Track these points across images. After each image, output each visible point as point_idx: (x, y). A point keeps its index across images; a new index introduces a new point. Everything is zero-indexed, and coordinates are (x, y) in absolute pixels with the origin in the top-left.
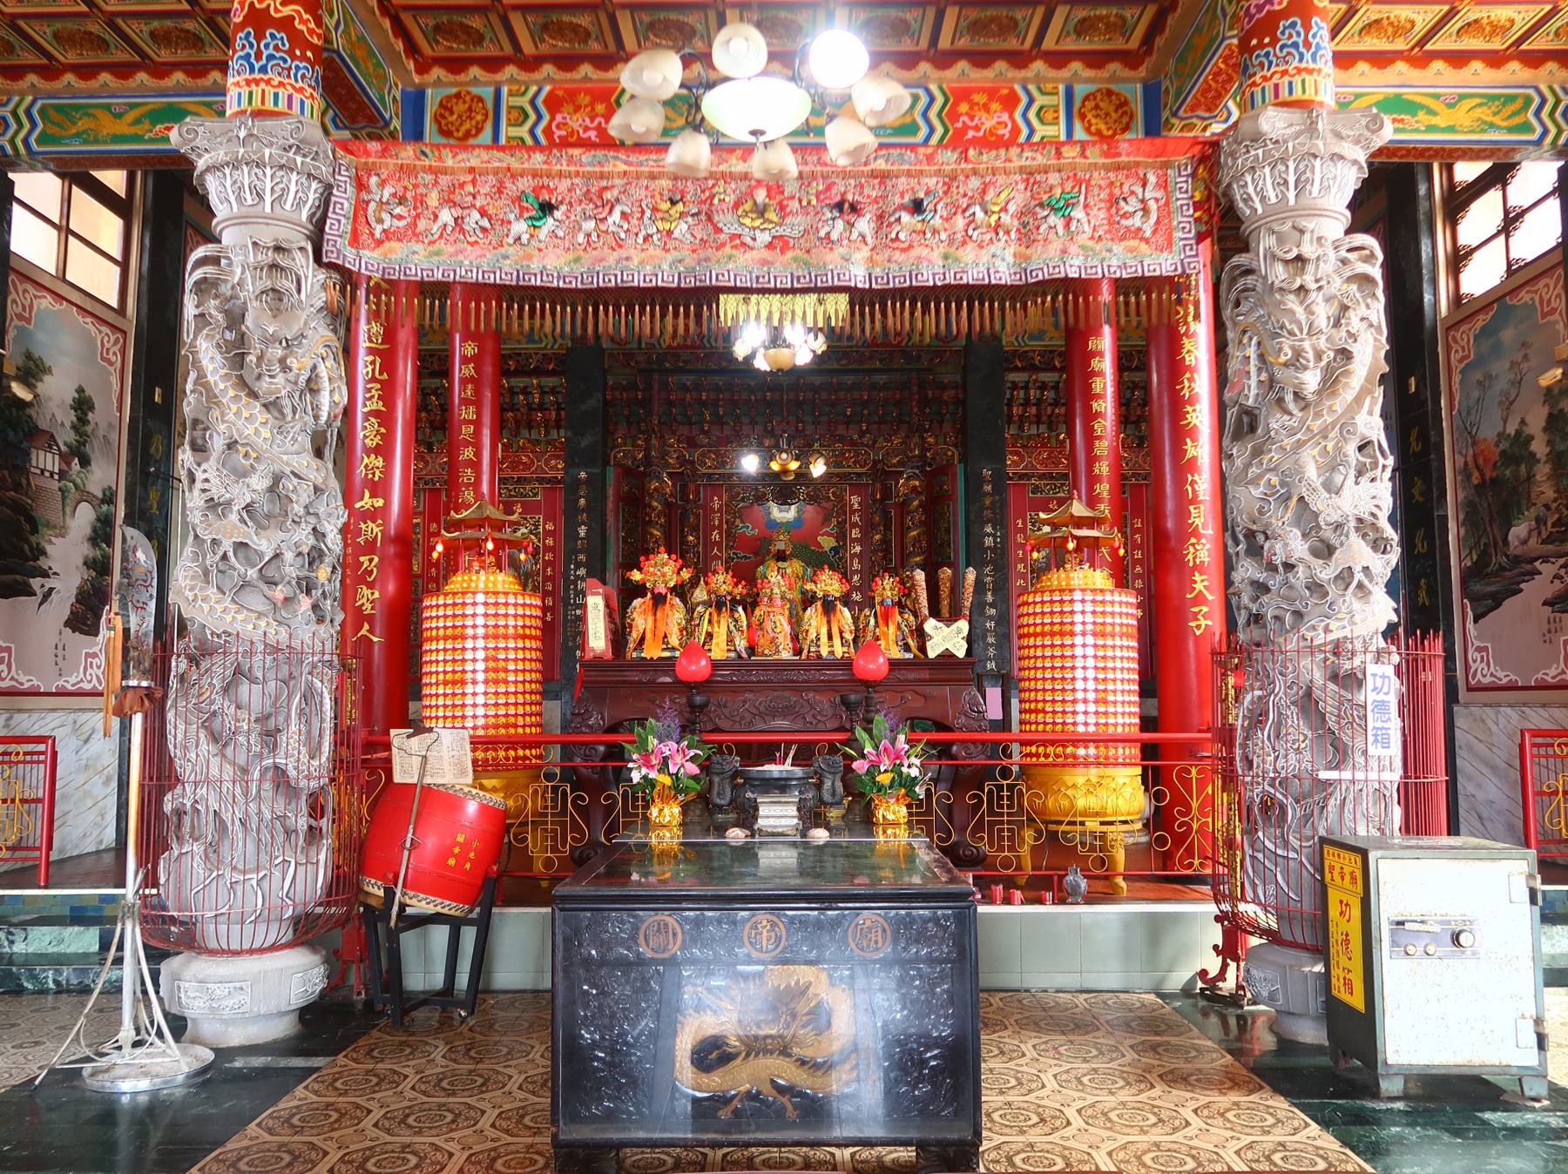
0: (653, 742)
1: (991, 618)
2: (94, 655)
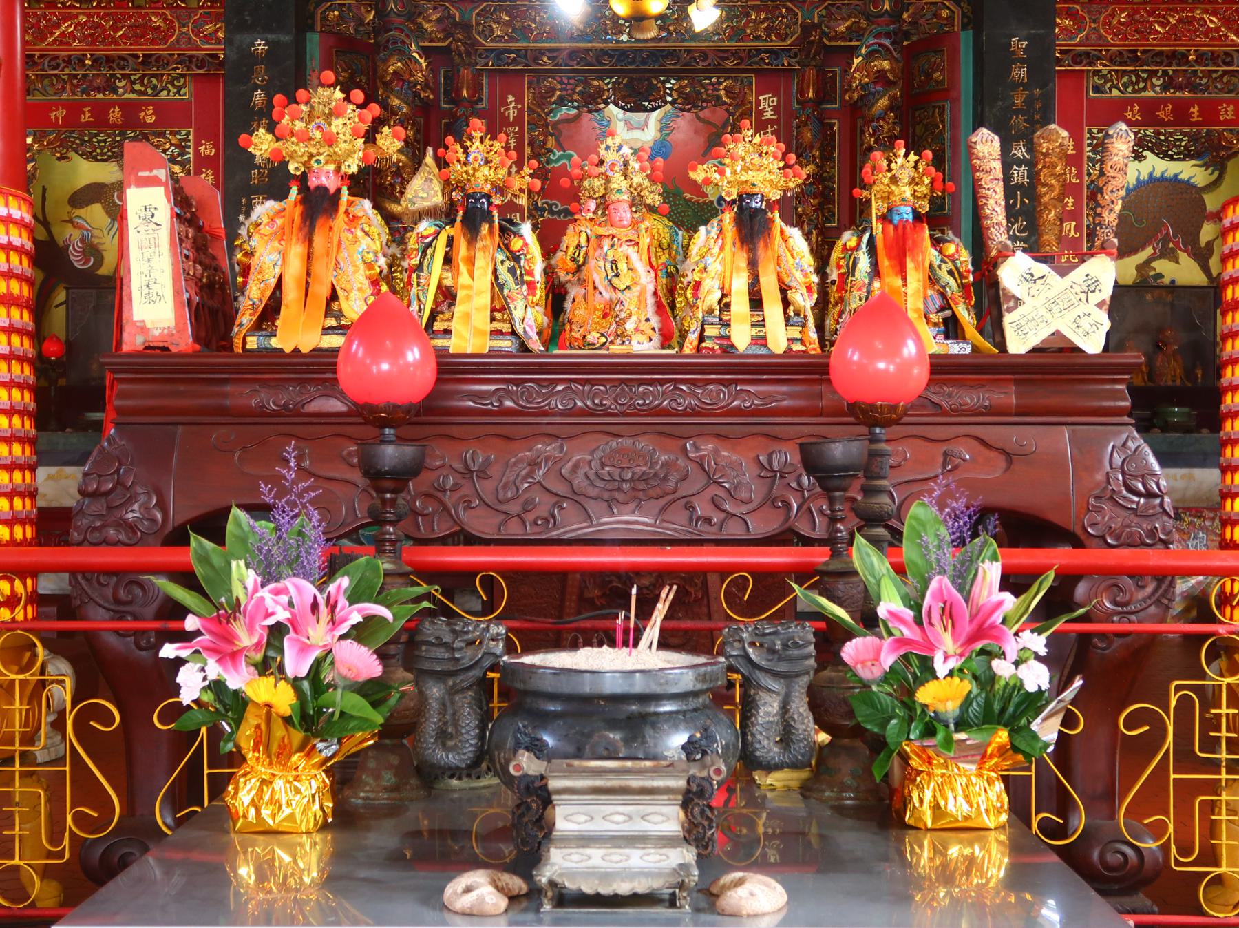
0: (243, 577)
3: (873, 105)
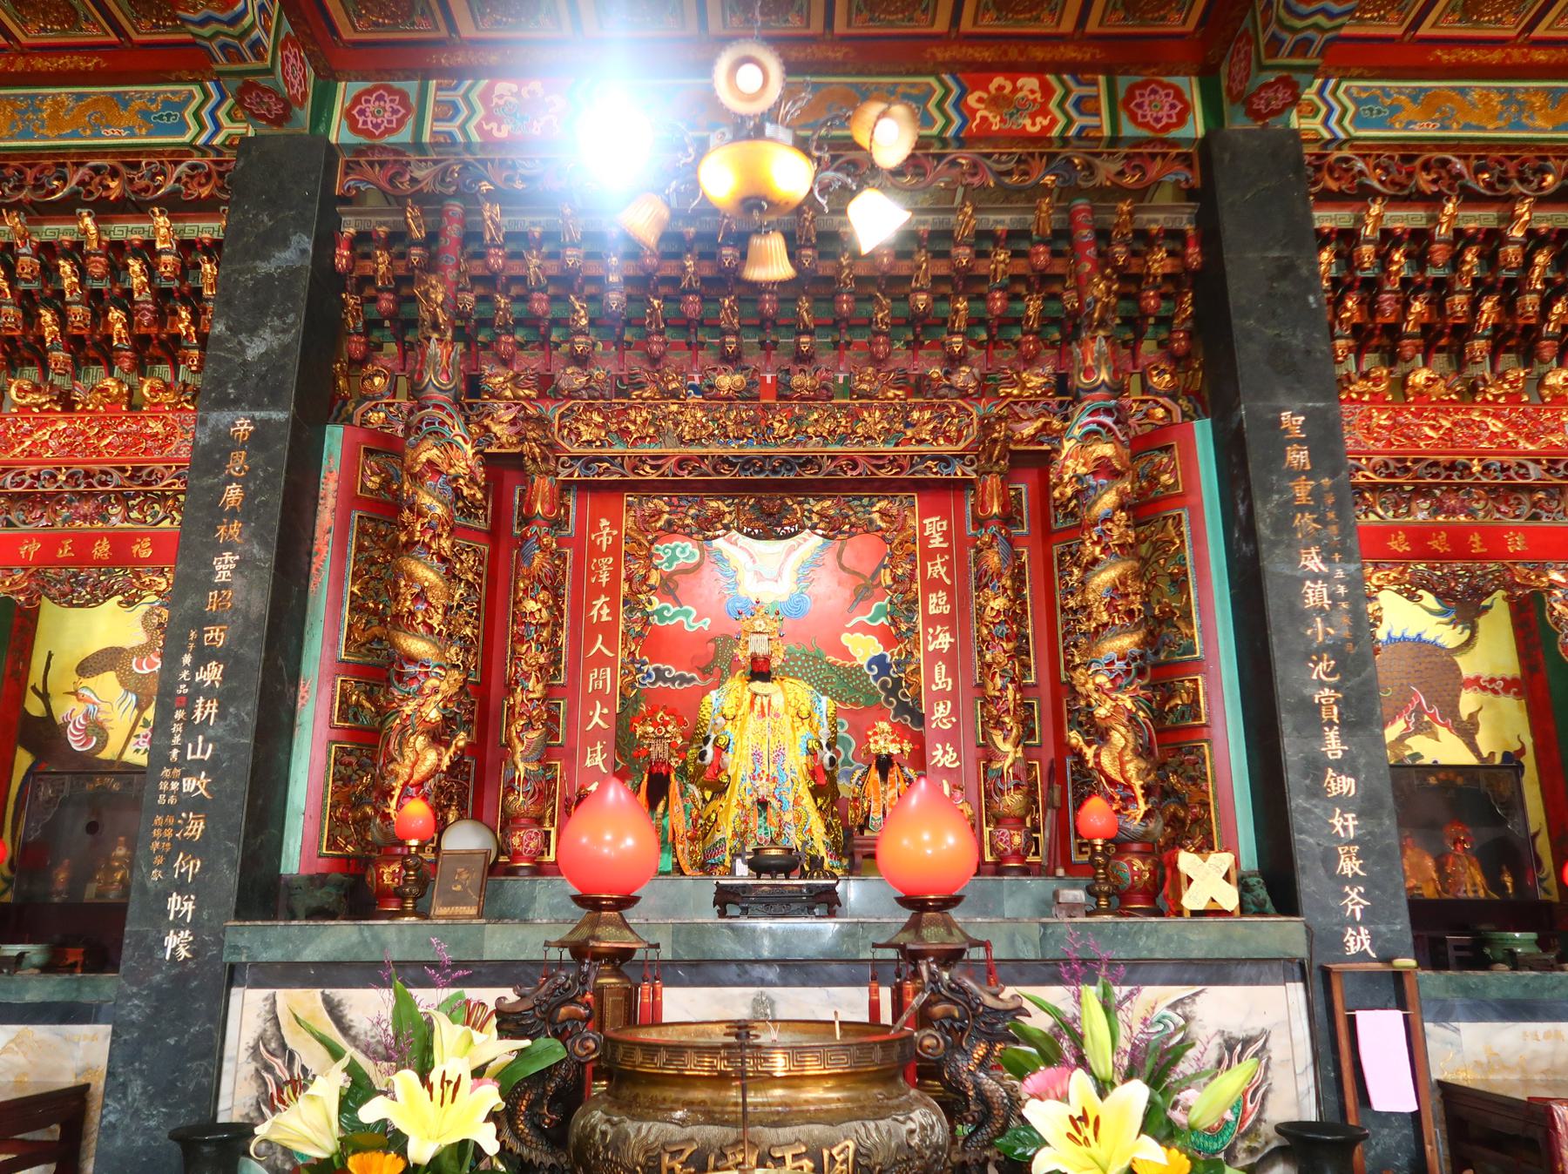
1: (1342, 802)
3: (1095, 502)
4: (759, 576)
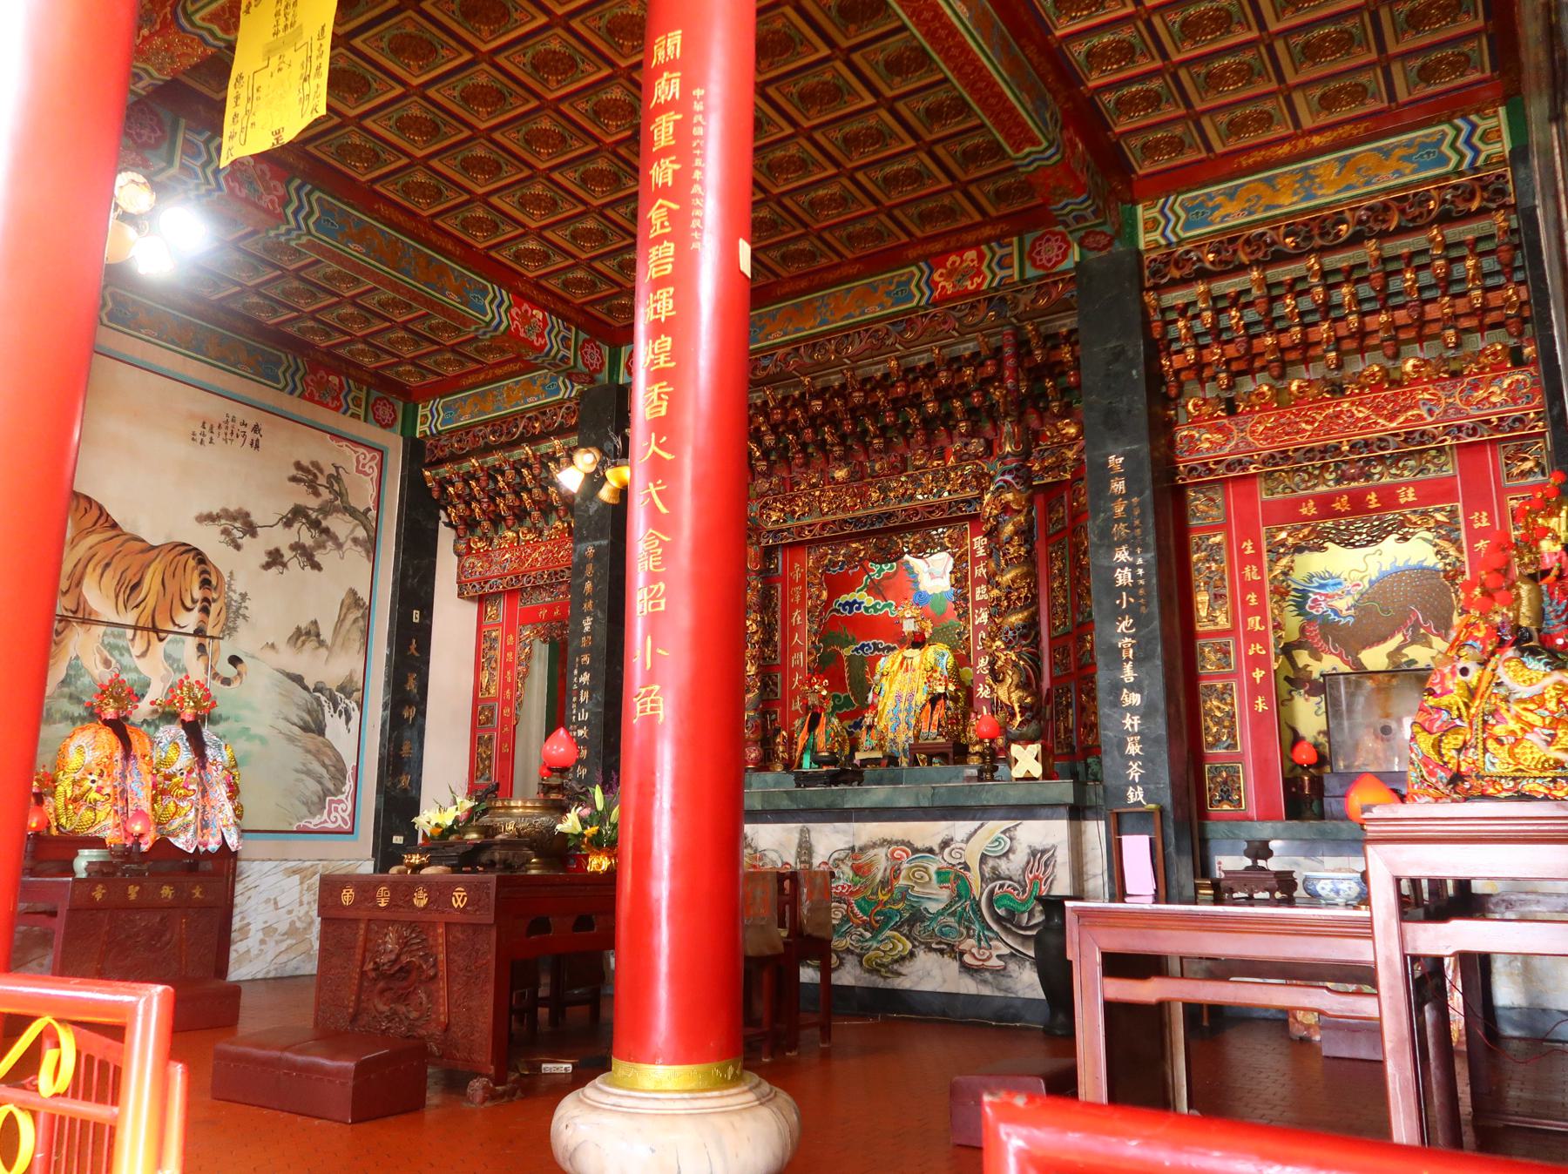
1: (1132, 710)
2: (341, 801)
4: (932, 576)
